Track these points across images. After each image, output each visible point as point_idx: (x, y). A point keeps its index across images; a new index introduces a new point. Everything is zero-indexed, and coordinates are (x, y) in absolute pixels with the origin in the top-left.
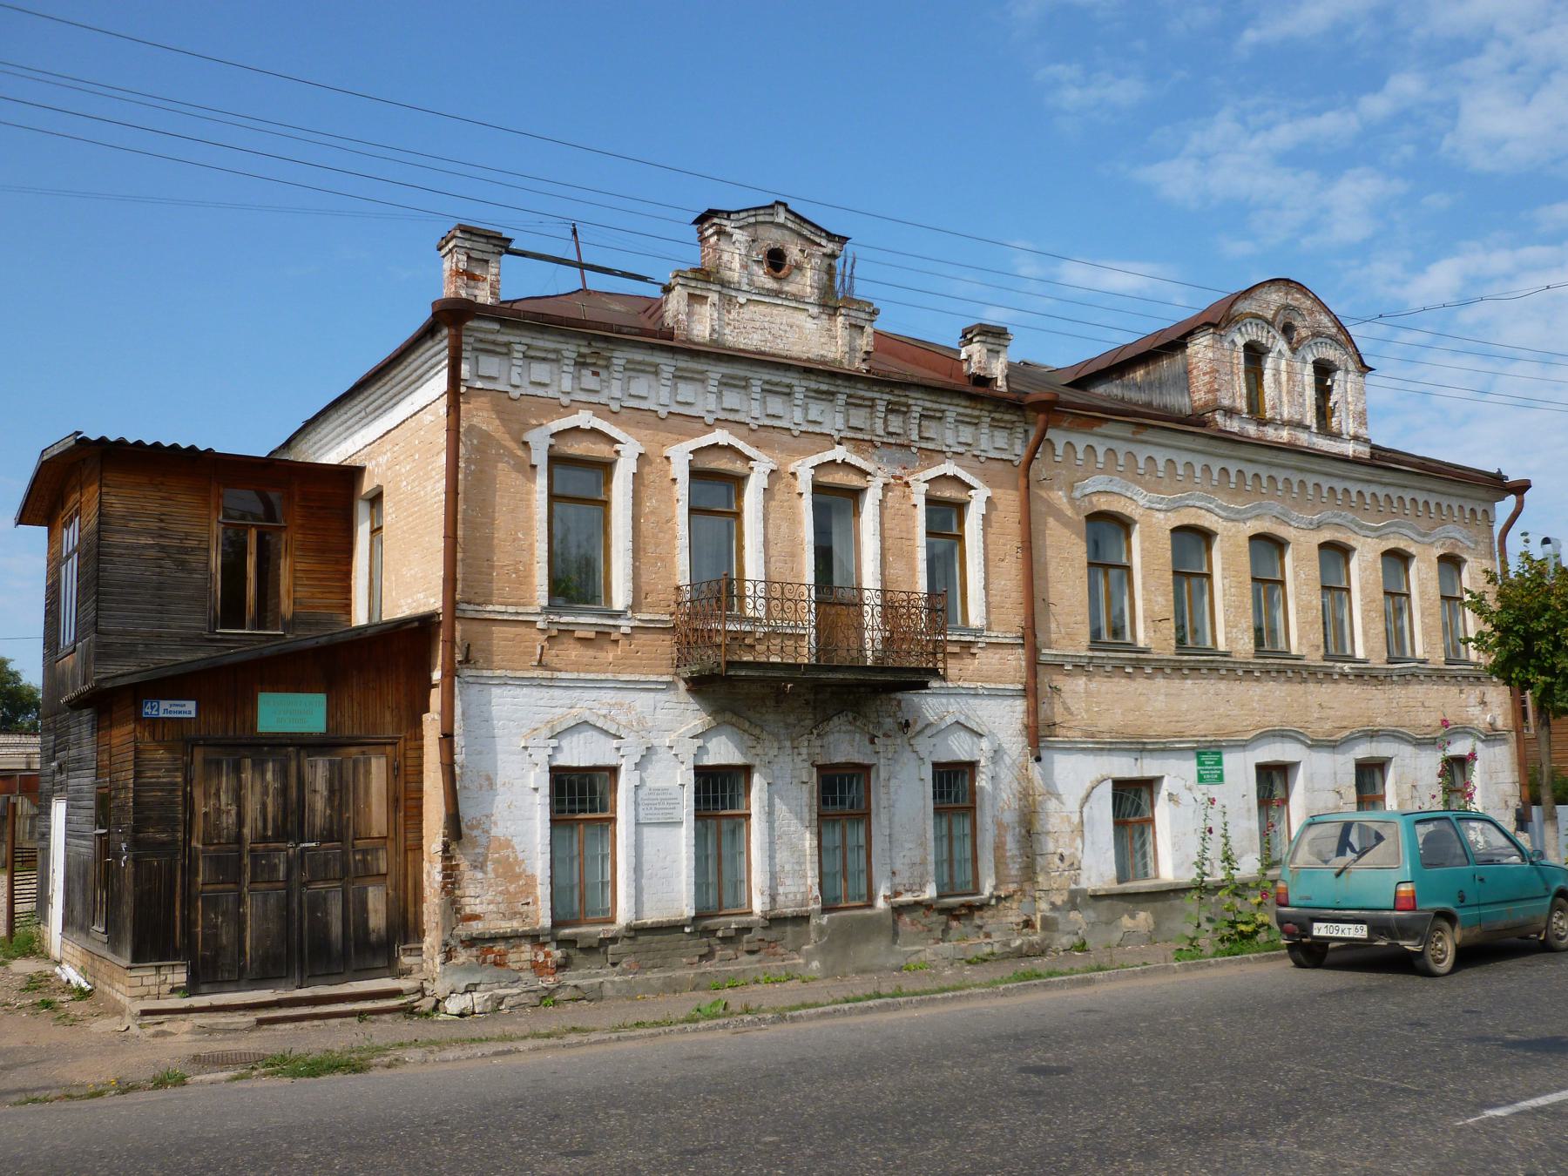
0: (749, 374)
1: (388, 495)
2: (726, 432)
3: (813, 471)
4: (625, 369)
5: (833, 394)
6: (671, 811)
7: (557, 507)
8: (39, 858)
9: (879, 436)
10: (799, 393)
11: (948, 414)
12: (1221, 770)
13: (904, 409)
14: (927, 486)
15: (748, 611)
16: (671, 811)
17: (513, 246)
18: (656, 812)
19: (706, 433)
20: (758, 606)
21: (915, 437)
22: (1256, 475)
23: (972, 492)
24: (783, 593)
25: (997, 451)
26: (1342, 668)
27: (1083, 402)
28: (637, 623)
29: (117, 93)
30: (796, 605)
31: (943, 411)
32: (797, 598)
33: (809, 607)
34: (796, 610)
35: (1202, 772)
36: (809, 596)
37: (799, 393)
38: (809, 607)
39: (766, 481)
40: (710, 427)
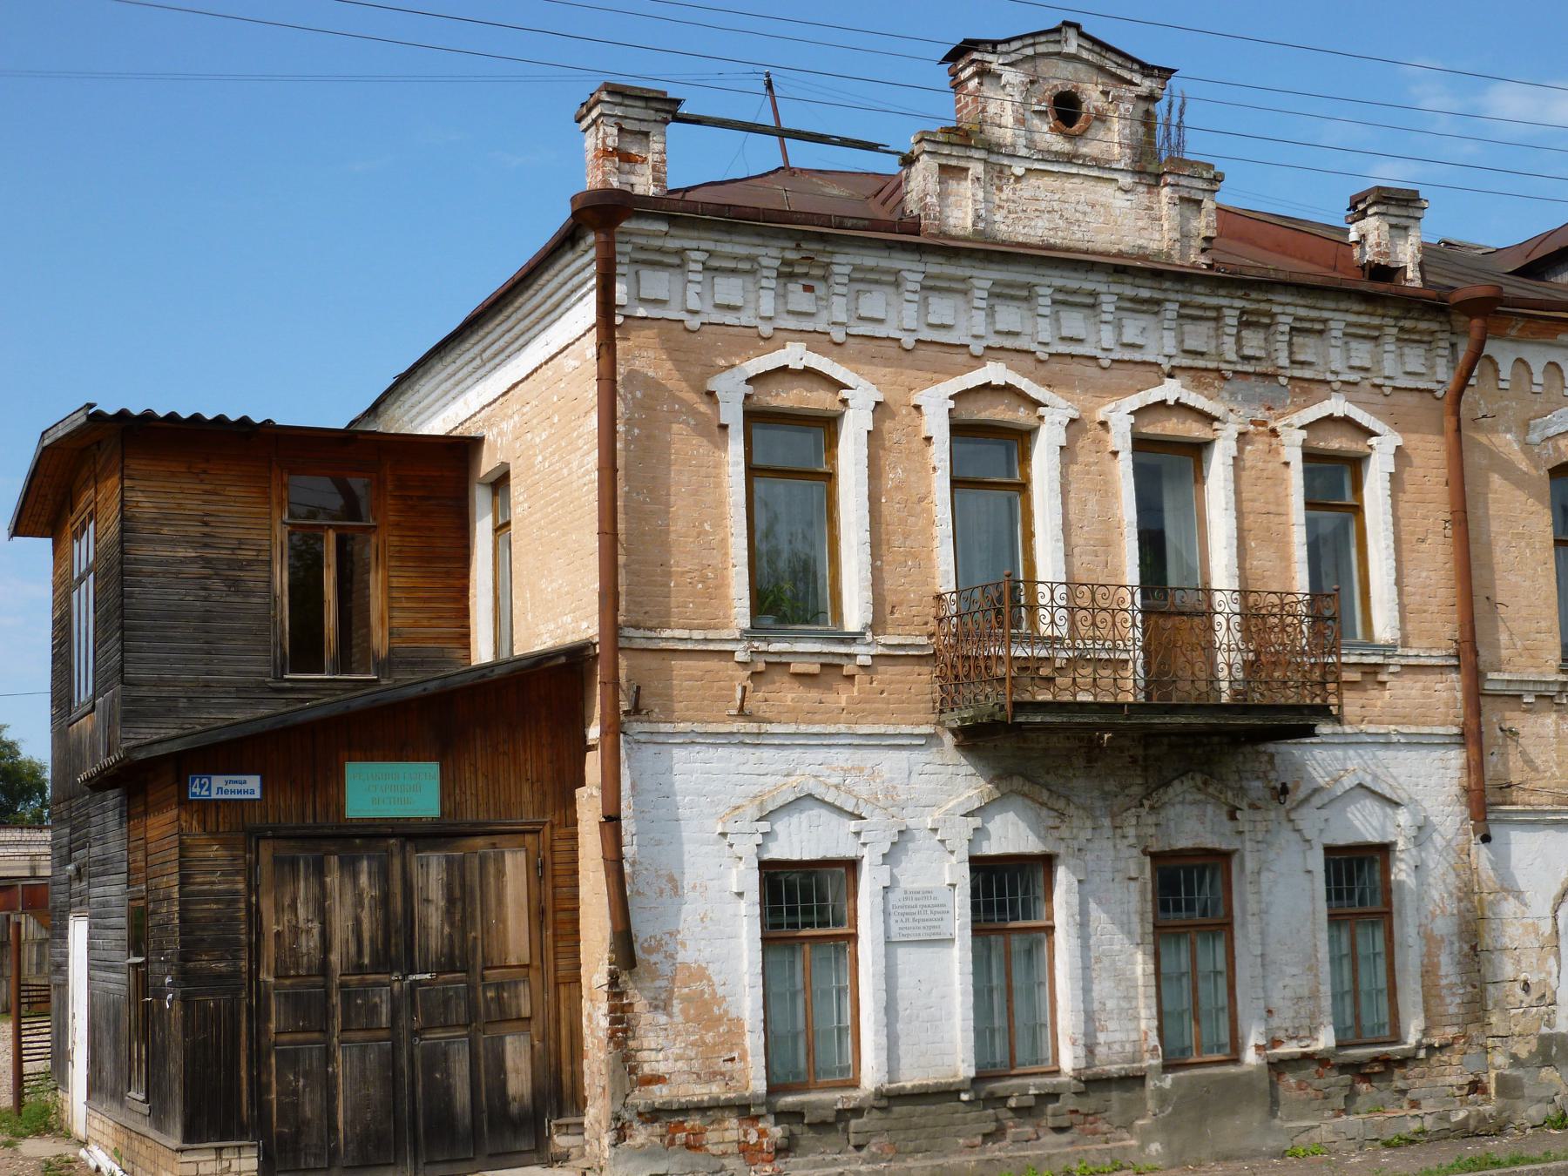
2: (1001, 366)
3: (1132, 419)
6: (935, 924)
10: (1108, 304)
11: (1332, 324)
16: (935, 924)
23: (1373, 441)
24: (1093, 600)
27: (1539, 297)
31: (1325, 321)
32: (1115, 606)
34: (1114, 624)
37: (1108, 304)
40: (978, 360)
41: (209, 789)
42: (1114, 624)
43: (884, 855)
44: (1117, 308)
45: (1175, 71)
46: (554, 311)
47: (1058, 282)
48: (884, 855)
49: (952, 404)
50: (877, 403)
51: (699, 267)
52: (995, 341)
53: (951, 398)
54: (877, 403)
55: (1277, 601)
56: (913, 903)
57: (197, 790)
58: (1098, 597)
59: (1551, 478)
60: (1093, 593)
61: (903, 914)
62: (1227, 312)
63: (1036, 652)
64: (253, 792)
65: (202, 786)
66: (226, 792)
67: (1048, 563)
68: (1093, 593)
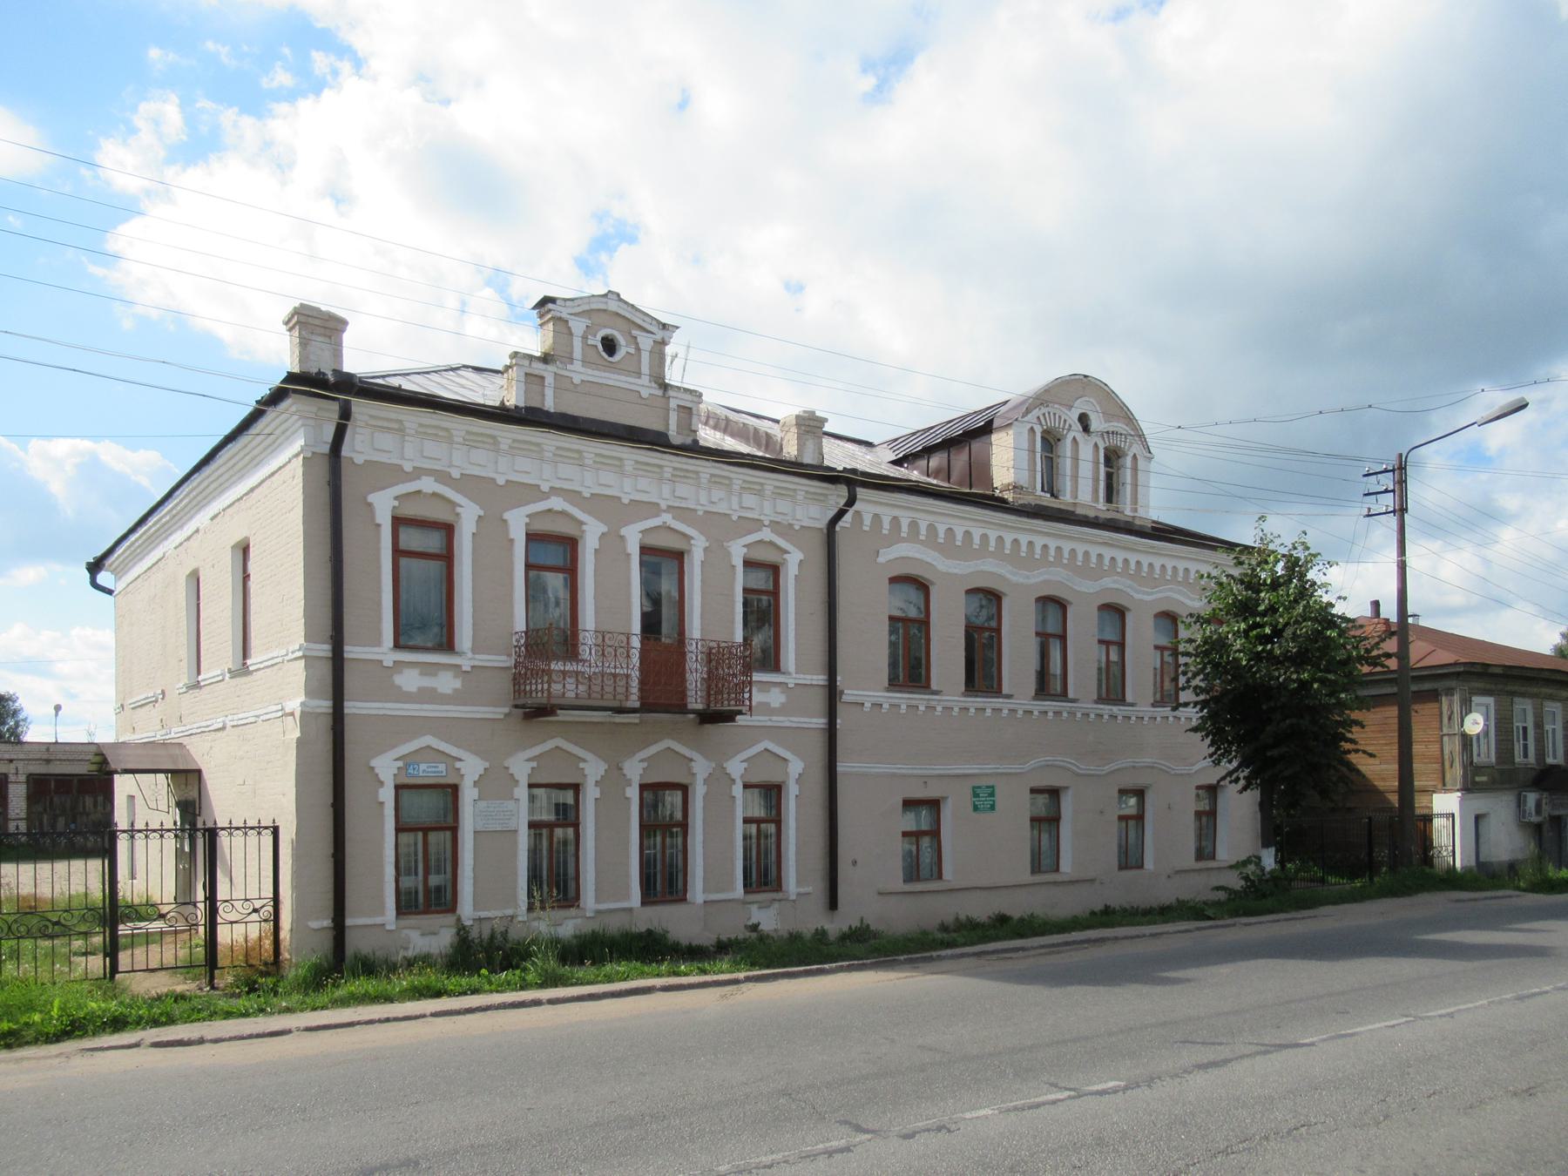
0: (582, 448)
1: (253, 546)
2: (561, 500)
3: (640, 535)
4: (416, 432)
5: (826, 495)
6: (506, 821)
7: (404, 561)
8: (767, 888)
9: (702, 505)
10: (800, 496)
11: (766, 487)
12: (994, 801)
13: (727, 482)
14: (745, 550)
15: (1517, 760)
16: (506, 821)
17: (827, 428)
18: (494, 822)
19: (542, 500)
20: (606, 653)
21: (735, 506)
22: (1016, 541)
23: (786, 556)
24: (604, 640)
25: (811, 521)
26: (1111, 710)
27: (874, 472)
28: (477, 663)
29: (947, 407)
30: (616, 651)
31: (762, 484)
32: (617, 644)
33: (697, 657)
34: (616, 655)
35: (976, 803)
36: (697, 647)
37: (800, 496)
38: (697, 657)
39: (703, 554)
40: (544, 496)
41: (418, 771)
42: (616, 655)
43: (475, 782)
44: (805, 498)
45: (677, 328)
46: (273, 448)
47: (598, 451)
48: (475, 782)
49: (527, 520)
50: (480, 517)
51: (413, 432)
52: (558, 484)
53: (527, 516)
54: (480, 517)
55: (716, 646)
56: (492, 809)
57: (412, 772)
58: (606, 639)
59: (890, 583)
60: (604, 637)
61: (486, 816)
62: (626, 462)
63: (579, 667)
64: (442, 772)
65: (414, 769)
66: (428, 772)
67: (588, 620)
68: (604, 637)
